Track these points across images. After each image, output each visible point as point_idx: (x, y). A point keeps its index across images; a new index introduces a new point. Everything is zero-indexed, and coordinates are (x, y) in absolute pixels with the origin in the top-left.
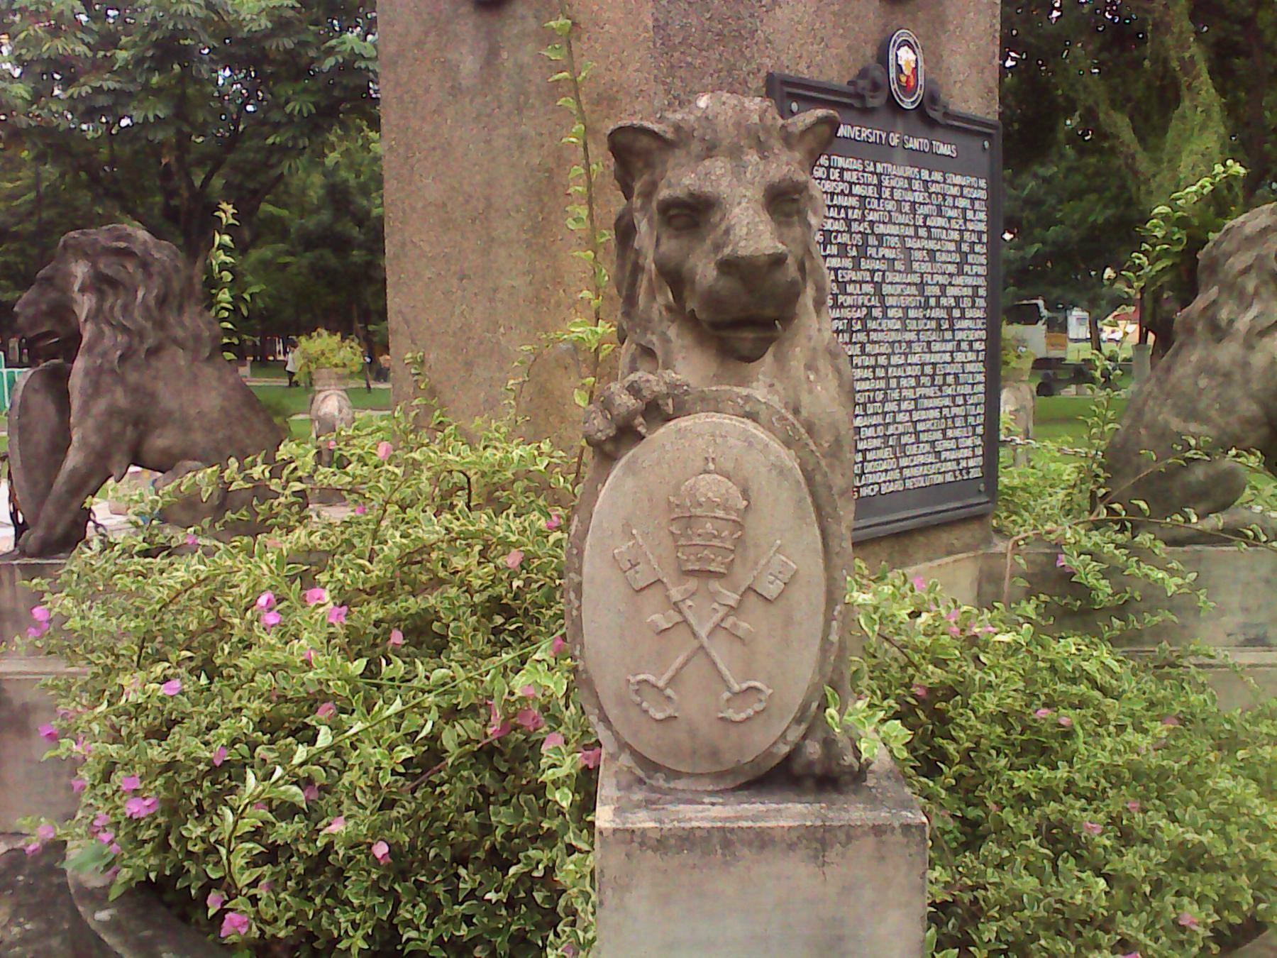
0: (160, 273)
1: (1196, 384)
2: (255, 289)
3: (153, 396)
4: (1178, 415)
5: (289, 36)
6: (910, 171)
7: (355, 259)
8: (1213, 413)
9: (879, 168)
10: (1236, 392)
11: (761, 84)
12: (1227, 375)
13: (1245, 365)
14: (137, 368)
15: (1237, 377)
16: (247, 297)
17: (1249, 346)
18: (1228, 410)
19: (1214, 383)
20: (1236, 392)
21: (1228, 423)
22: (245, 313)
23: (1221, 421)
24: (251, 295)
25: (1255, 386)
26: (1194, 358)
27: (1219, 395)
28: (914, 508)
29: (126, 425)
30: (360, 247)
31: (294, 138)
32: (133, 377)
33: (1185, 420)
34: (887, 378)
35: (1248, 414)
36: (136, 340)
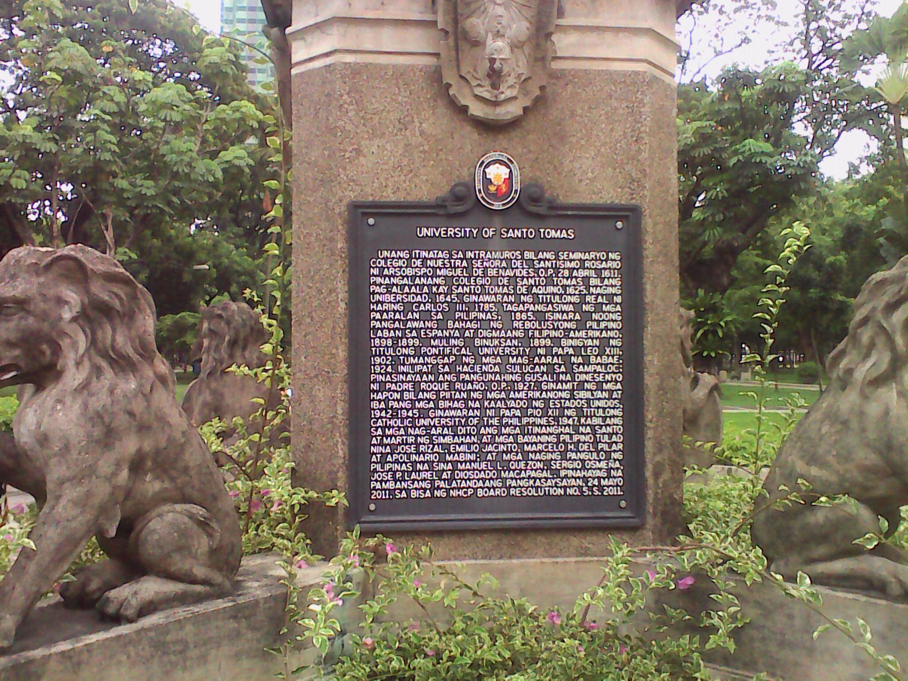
0: (234, 328)
1: (820, 430)
2: (729, 318)
3: (222, 395)
4: (802, 458)
5: (707, 145)
6: (508, 254)
7: (814, 296)
8: (830, 458)
9: (470, 255)
10: (852, 440)
11: (343, 209)
12: (845, 423)
13: (862, 414)
14: (216, 380)
15: (854, 425)
16: (722, 324)
17: (865, 397)
18: (846, 458)
19: (833, 430)
20: (852, 440)
21: (846, 471)
22: (721, 334)
23: (841, 468)
24: (726, 323)
25: (872, 435)
26: (824, 405)
27: (836, 442)
28: (523, 511)
29: (210, 411)
30: (816, 286)
31: (713, 215)
32: (213, 385)
33: (808, 464)
34: (482, 408)
35: (867, 462)
36: (219, 364)
